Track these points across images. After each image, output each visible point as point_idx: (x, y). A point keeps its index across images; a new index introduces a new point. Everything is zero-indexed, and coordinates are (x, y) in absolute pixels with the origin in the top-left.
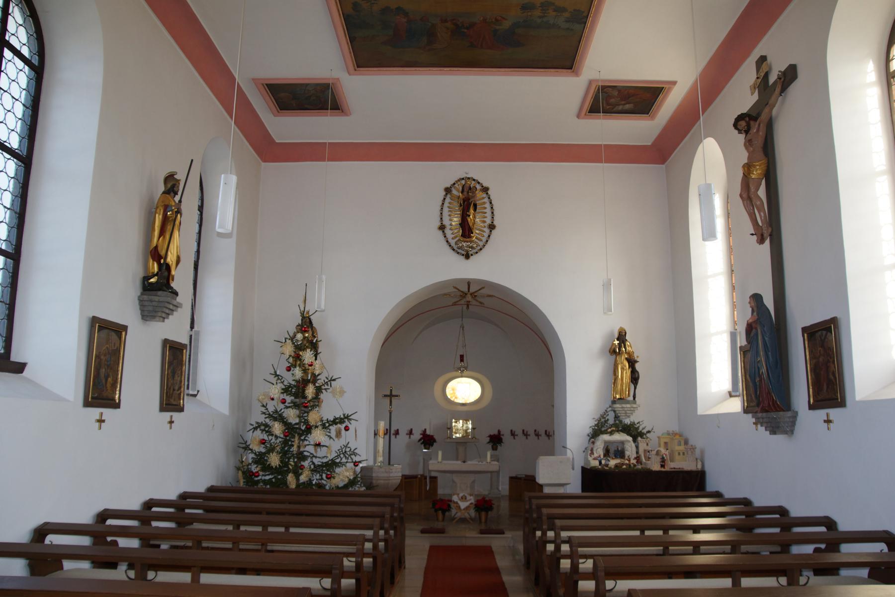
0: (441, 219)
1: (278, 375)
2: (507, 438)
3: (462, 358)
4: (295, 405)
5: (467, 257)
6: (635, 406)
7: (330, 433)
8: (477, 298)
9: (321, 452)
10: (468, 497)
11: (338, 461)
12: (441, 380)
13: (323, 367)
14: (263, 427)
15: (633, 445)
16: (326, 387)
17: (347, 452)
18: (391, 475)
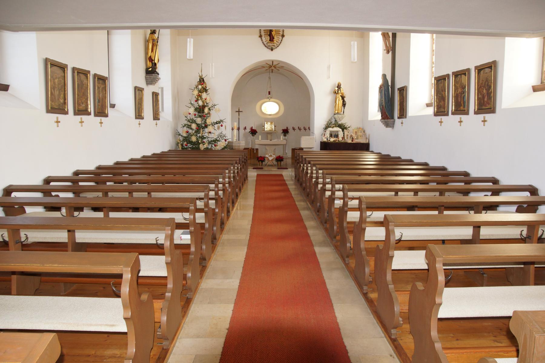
0: (260, 32)
1: (192, 104)
2: (290, 130)
3: (269, 93)
4: (200, 116)
5: (272, 50)
6: (343, 116)
7: (214, 127)
8: (276, 68)
9: (211, 136)
10: (273, 155)
11: (218, 139)
12: (259, 104)
13: (211, 99)
14: (187, 126)
15: (342, 133)
16: (212, 108)
17: (221, 136)
18: (241, 145)
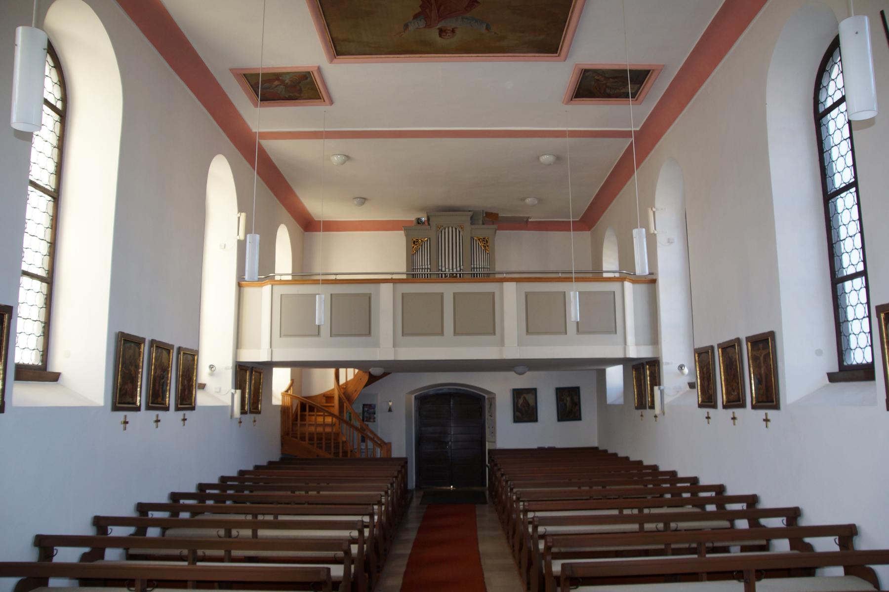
3: (857, 33)
